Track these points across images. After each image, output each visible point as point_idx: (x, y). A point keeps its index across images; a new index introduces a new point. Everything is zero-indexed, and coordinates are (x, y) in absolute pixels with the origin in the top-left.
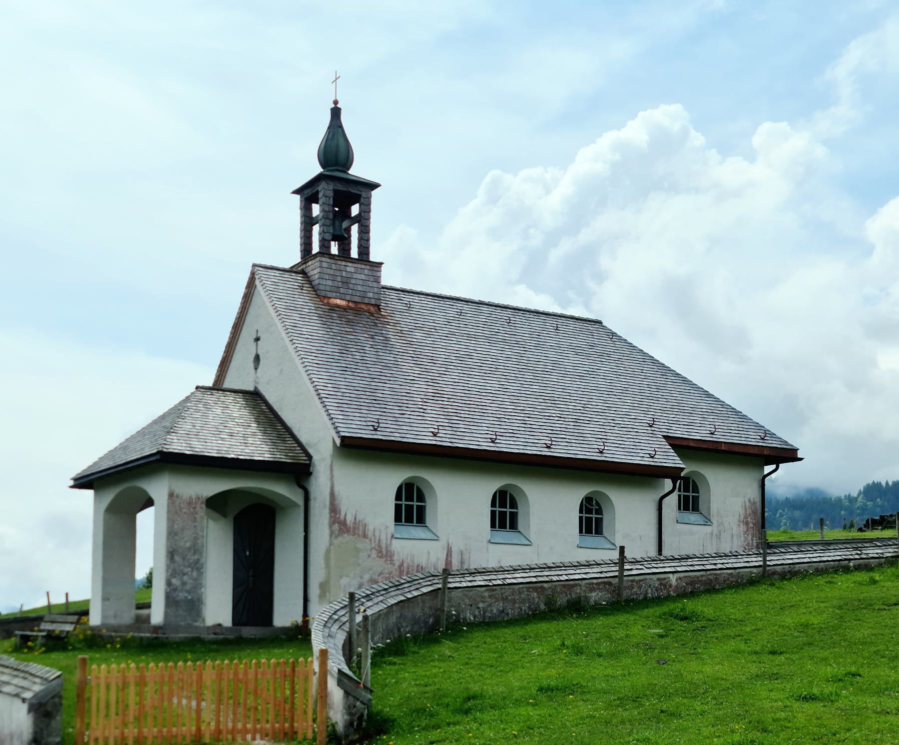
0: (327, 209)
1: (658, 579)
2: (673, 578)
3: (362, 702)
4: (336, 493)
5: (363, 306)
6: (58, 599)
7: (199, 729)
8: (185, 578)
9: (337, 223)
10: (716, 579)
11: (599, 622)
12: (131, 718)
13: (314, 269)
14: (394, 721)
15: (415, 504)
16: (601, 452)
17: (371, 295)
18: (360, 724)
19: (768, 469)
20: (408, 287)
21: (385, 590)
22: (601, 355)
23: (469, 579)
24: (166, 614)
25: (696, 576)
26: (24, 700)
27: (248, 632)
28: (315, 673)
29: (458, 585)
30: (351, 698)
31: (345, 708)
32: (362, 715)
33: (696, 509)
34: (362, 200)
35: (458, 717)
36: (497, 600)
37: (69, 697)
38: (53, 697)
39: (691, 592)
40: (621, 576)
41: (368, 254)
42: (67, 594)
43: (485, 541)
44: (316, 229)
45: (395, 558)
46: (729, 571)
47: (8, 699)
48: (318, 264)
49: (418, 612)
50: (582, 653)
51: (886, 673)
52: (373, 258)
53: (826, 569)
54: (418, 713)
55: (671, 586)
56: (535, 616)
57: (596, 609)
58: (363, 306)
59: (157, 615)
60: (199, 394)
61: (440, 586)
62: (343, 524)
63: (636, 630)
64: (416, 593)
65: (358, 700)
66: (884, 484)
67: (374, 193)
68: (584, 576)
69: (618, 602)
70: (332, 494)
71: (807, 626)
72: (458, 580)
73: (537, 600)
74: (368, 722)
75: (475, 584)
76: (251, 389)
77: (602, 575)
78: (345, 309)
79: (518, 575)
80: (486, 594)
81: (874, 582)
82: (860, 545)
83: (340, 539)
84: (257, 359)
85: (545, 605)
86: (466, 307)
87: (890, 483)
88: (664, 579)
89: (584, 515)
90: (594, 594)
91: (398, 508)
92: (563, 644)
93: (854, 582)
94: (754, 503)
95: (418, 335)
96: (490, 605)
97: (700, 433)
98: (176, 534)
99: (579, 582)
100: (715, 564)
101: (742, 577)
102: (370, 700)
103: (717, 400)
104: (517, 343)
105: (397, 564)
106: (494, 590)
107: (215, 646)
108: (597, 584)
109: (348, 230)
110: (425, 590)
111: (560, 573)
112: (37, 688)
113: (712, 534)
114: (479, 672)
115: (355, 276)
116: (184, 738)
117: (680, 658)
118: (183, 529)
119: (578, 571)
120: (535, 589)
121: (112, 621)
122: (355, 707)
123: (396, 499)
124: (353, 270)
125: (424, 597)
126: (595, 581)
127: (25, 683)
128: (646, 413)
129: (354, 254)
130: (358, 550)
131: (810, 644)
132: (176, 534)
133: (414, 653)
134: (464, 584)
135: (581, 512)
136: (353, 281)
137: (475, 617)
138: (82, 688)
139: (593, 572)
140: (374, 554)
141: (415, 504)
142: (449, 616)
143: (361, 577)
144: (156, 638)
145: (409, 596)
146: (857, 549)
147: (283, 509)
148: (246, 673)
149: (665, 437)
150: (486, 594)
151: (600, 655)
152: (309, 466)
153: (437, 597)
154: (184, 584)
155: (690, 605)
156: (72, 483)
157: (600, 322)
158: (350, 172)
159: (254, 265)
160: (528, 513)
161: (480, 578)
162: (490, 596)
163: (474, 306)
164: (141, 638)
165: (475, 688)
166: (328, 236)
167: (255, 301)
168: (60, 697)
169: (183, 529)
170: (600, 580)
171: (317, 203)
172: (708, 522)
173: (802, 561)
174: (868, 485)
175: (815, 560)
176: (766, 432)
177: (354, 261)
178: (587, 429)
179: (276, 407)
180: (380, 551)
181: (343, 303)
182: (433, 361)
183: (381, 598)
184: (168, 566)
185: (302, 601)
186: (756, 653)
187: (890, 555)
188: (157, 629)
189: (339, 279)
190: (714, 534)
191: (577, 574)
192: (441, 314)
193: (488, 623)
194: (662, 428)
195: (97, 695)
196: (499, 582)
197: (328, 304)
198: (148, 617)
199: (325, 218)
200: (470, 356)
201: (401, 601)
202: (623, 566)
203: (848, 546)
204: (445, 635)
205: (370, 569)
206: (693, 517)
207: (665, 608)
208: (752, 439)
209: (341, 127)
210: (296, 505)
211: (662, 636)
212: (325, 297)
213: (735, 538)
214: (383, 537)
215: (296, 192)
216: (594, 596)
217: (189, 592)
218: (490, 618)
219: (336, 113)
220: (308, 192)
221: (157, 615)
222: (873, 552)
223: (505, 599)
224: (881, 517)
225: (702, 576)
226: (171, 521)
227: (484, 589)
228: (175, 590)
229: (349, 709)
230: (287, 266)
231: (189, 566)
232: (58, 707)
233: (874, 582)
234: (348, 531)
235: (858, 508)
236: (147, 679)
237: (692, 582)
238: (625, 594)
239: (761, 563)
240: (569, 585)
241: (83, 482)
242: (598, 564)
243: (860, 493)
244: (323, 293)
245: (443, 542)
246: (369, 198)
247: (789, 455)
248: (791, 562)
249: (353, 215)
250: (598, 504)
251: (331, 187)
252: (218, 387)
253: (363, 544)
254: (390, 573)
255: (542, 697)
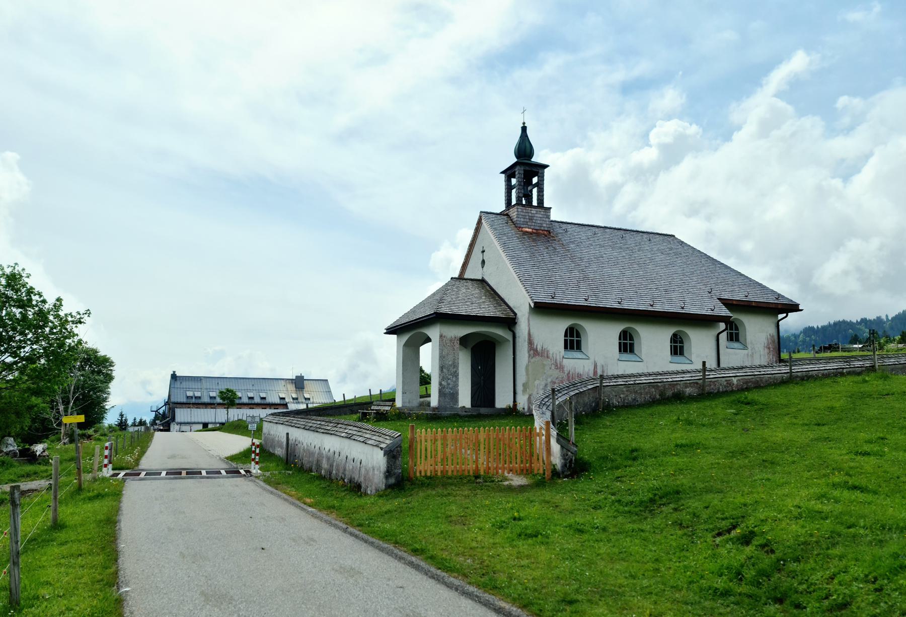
0: (520, 180)
1: (726, 381)
2: (735, 380)
3: (571, 453)
4: (531, 334)
5: (541, 232)
6: (375, 392)
7: (477, 467)
8: (449, 381)
9: (525, 188)
10: (761, 380)
11: (694, 406)
12: (439, 460)
13: (513, 213)
14: (590, 463)
15: (575, 339)
16: (683, 308)
17: (545, 225)
18: (570, 466)
19: (780, 316)
20: (565, 221)
21: (567, 387)
22: (676, 254)
23: (614, 381)
24: (439, 401)
25: (748, 379)
26: (381, 449)
27: (483, 410)
28: (543, 435)
29: (608, 384)
30: (564, 450)
31: (561, 455)
32: (571, 460)
33: (737, 340)
34: (539, 174)
35: (630, 462)
36: (631, 393)
37: (405, 446)
38: (397, 447)
39: (746, 388)
40: (704, 379)
41: (543, 203)
42: (370, 390)
43: (616, 359)
44: (514, 192)
45: (565, 369)
46: (769, 376)
47: (370, 448)
48: (516, 210)
49: (586, 400)
50: (692, 424)
51: (898, 437)
52: (546, 205)
53: (829, 374)
54: (603, 459)
55: (733, 384)
56: (653, 403)
57: (691, 398)
58: (541, 232)
59: (434, 401)
60: (453, 282)
61: (598, 385)
62: (536, 351)
63: (718, 410)
64: (585, 389)
65: (569, 451)
66: (855, 322)
67: (546, 170)
68: (682, 379)
69: (702, 394)
70: (529, 334)
71: (832, 408)
72: (608, 381)
73: (654, 393)
74: (575, 464)
75: (618, 383)
76: (481, 278)
77: (692, 378)
78: (531, 233)
79: (643, 379)
80: (625, 389)
81: (865, 381)
82: (848, 360)
83: (534, 359)
84: (483, 262)
85: (660, 395)
86: (597, 230)
87: (820, 327)
88: (730, 380)
89: (673, 344)
90: (688, 389)
91: (566, 341)
92: (679, 419)
93: (853, 382)
94: (773, 336)
95: (572, 246)
96: (627, 396)
97: (739, 296)
98: (444, 357)
99: (679, 382)
100: (760, 372)
101: (777, 379)
102: (576, 451)
103: (747, 277)
104: (628, 248)
105: (566, 372)
106: (629, 387)
107: (467, 419)
108: (689, 383)
109: (531, 191)
110: (590, 387)
111: (667, 377)
112: (388, 442)
113: (748, 355)
114: (631, 435)
115: (536, 215)
116: (469, 472)
117: (757, 427)
118: (448, 354)
119: (678, 376)
120: (653, 387)
121: (408, 405)
122: (567, 455)
123: (565, 337)
124: (535, 212)
125: (589, 391)
126: (688, 382)
127: (381, 439)
128: (705, 285)
129: (535, 203)
130: (544, 365)
131: (841, 419)
132: (444, 357)
133: (587, 423)
134: (612, 384)
135: (671, 343)
136: (535, 218)
137: (619, 402)
138: (412, 441)
139: (687, 377)
140: (553, 367)
141: (575, 339)
142: (604, 402)
143: (546, 380)
144: (435, 414)
145: (582, 391)
146: (847, 362)
147: (499, 342)
148: (503, 435)
149: (718, 299)
150: (625, 389)
151: (704, 425)
152: (515, 318)
153: (596, 391)
154: (448, 384)
155: (750, 396)
156: (385, 331)
157: (674, 236)
158: (532, 160)
159: (481, 212)
160: (640, 343)
161: (620, 380)
162: (627, 391)
163: (602, 229)
164: (427, 414)
165: (634, 445)
166: (521, 195)
167: (482, 231)
168: (401, 447)
169: (448, 354)
170: (691, 381)
171: (514, 177)
172: (745, 347)
173: (814, 369)
174: (806, 328)
175: (821, 369)
176: (779, 295)
177: (535, 207)
178: (674, 295)
179: (494, 287)
180: (557, 366)
181: (530, 230)
182: (581, 259)
183: (566, 392)
184: (440, 375)
185: (512, 394)
186: (807, 425)
187: (868, 365)
188: (434, 409)
189: (527, 217)
190: (749, 354)
191: (678, 378)
192: (584, 234)
193: (627, 407)
194: (716, 293)
195: (419, 448)
196: (632, 383)
197: (522, 231)
198: (429, 404)
199: (519, 185)
200: (602, 257)
201: (577, 393)
202: (705, 372)
203: (841, 360)
204: (603, 412)
205: (551, 376)
206: (736, 345)
207: (733, 398)
208: (771, 299)
209: (527, 136)
210: (508, 340)
211: (736, 414)
212: (520, 227)
213: (762, 357)
214: (558, 358)
215: (502, 173)
216: (688, 391)
217: (451, 389)
218: (627, 403)
219: (524, 129)
220: (509, 172)
221: (434, 401)
222: (857, 364)
223: (636, 392)
224: (829, 345)
225: (752, 378)
226: (441, 350)
227: (623, 386)
228: (444, 388)
229: (564, 456)
230: (499, 212)
231: (451, 375)
232: (399, 452)
233: (865, 381)
234: (538, 355)
235: (800, 342)
236: (448, 437)
237: (747, 382)
238: (707, 389)
239: (789, 371)
240: (673, 384)
241: (391, 331)
242: (689, 372)
243: (801, 332)
244: (519, 226)
245: (592, 360)
246: (543, 173)
247: (794, 308)
248: (807, 370)
249: (534, 183)
250: (680, 338)
251: (522, 168)
252: (461, 278)
253: (547, 362)
254: (562, 378)
255: (679, 450)
